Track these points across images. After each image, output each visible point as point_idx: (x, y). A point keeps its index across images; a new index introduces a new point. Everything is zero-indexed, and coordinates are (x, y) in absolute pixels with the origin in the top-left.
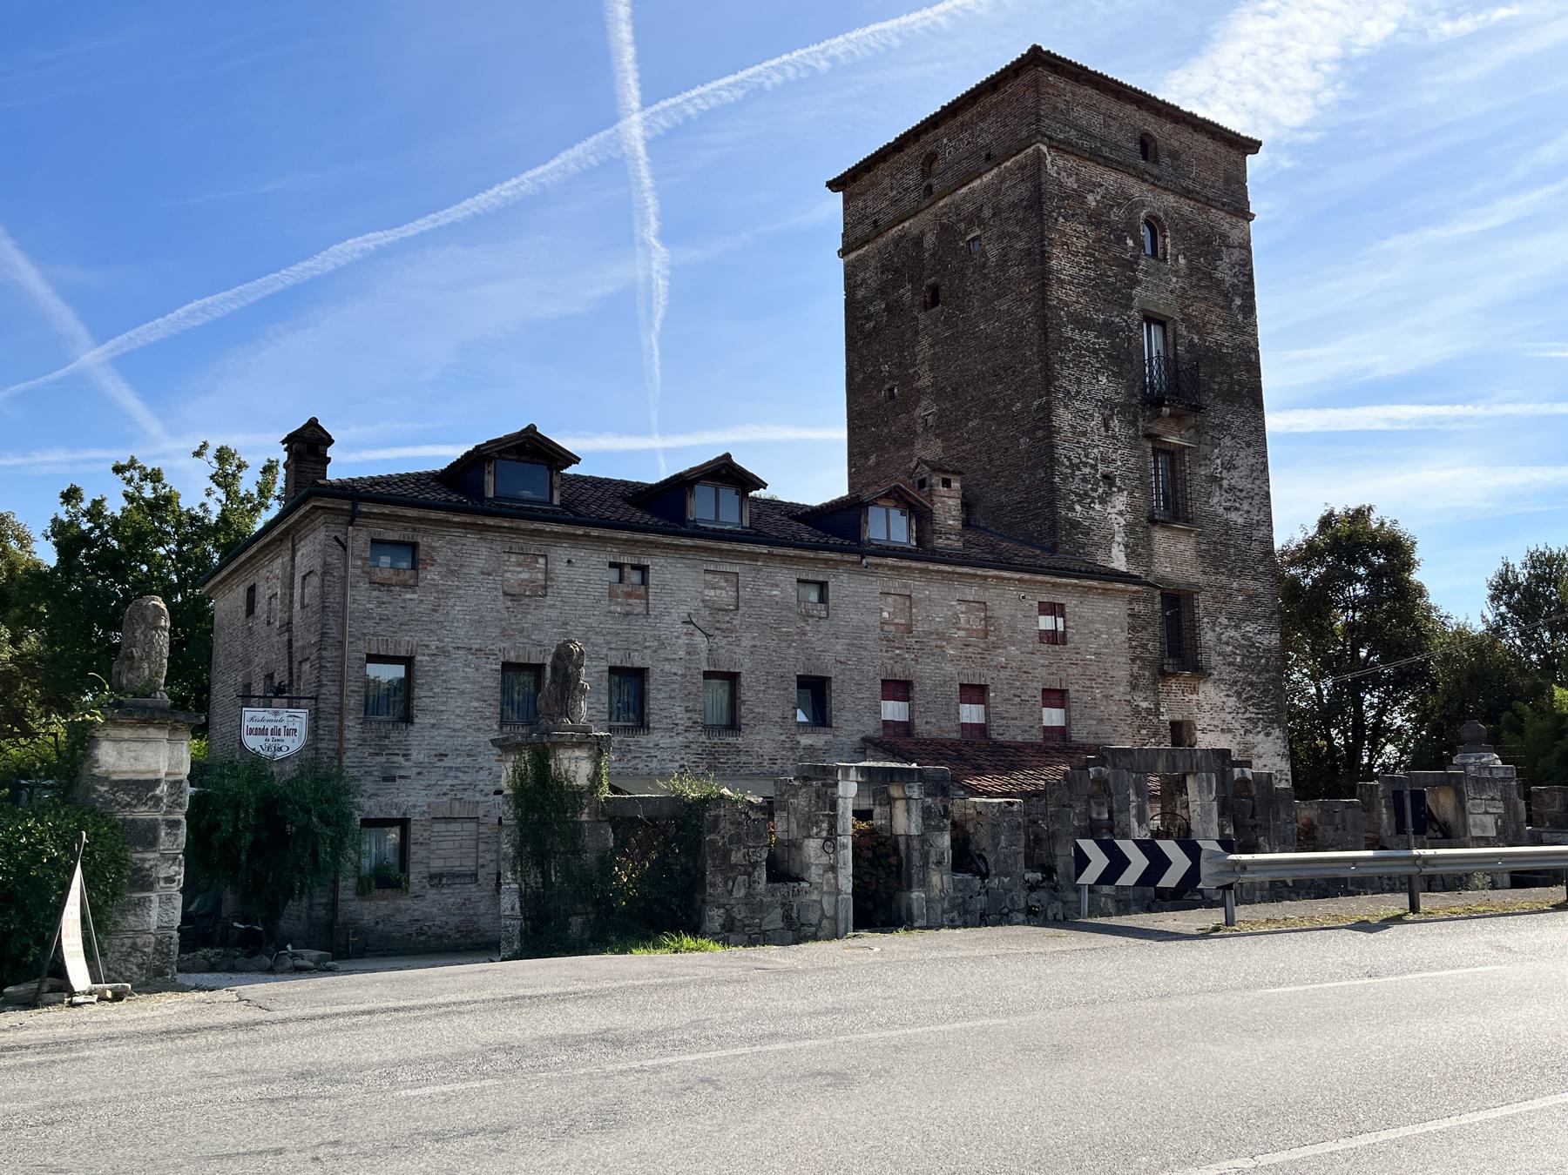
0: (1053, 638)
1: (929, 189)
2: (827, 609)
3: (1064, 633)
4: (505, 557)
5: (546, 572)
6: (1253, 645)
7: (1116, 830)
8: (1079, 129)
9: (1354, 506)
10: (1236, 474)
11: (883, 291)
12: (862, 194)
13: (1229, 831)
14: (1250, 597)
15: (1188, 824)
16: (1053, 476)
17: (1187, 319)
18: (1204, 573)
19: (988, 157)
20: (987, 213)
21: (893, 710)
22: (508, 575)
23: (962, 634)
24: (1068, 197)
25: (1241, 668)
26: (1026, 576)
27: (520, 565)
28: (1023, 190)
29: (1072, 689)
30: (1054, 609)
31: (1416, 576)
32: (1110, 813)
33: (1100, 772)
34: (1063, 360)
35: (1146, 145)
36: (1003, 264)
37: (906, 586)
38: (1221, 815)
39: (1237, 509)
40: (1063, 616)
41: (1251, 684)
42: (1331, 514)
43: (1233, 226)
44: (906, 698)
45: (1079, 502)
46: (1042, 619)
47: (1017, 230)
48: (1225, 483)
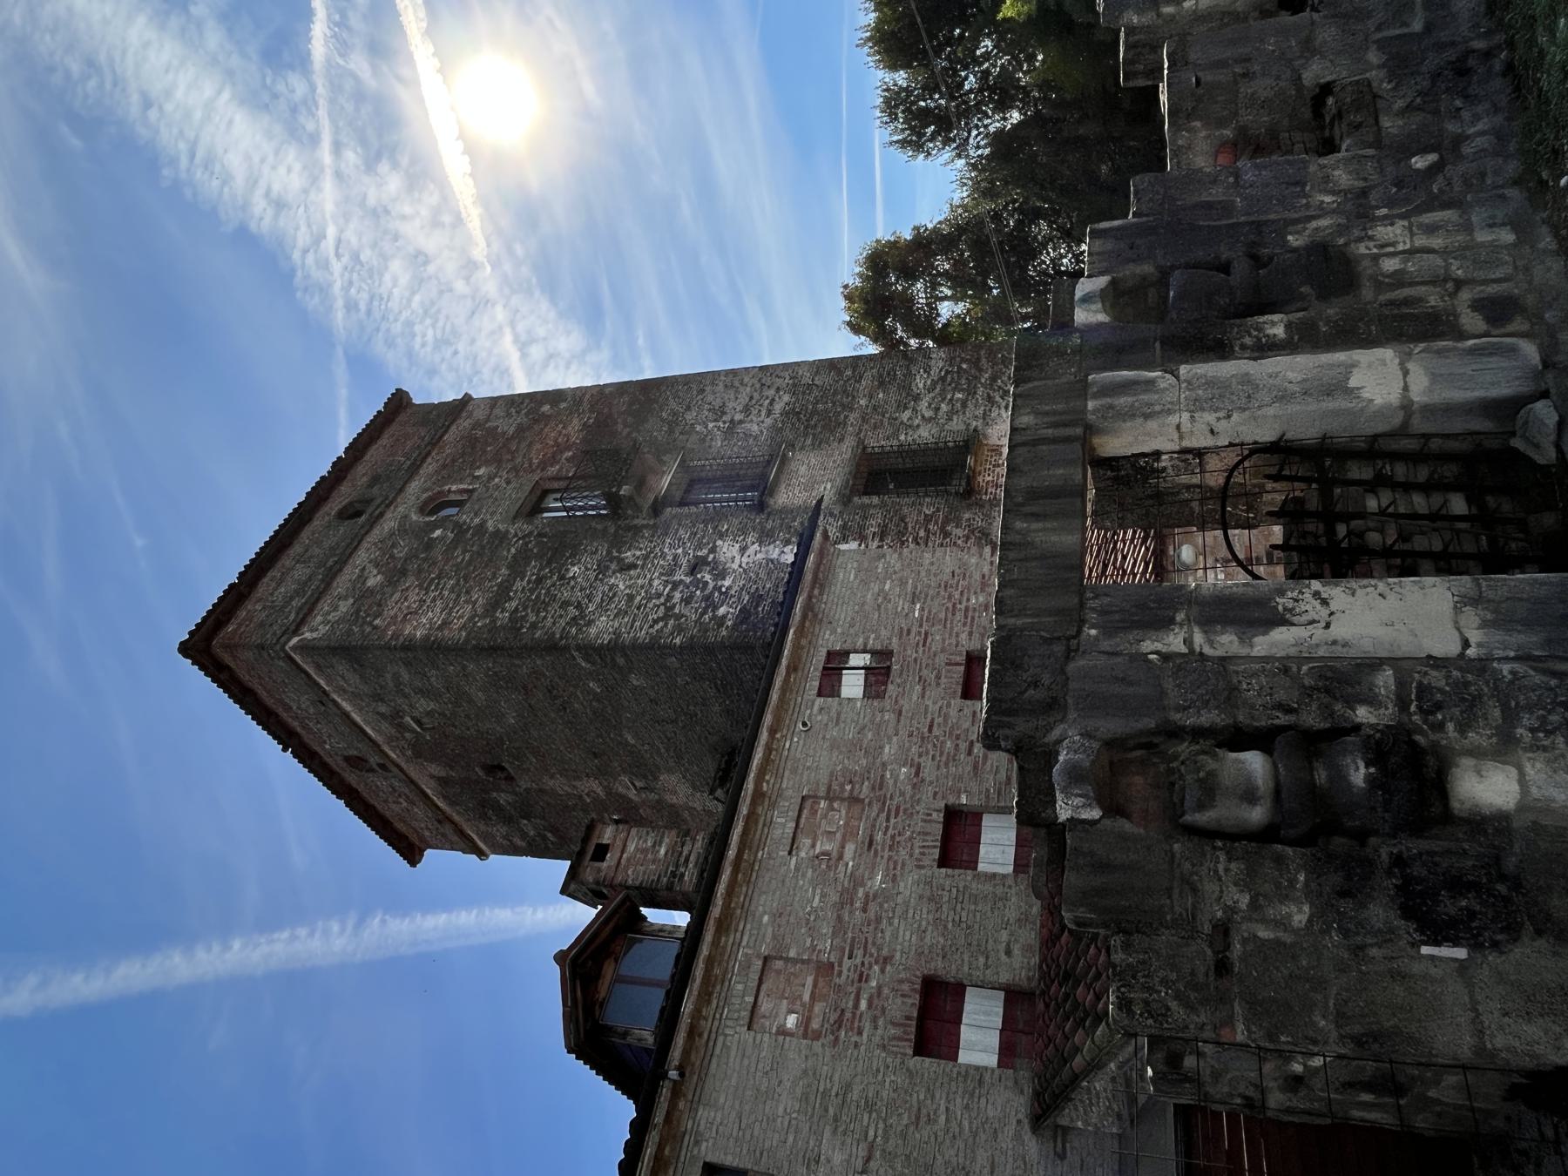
0: (877, 676)
3: (873, 653)
6: (943, 379)
7: (1311, 719)
8: (297, 593)
9: (843, 303)
10: (731, 405)
13: (1275, 325)
14: (882, 384)
15: (1259, 449)
16: (671, 647)
17: (543, 465)
18: (841, 440)
21: (980, 1034)
23: (850, 849)
25: (971, 392)
26: (768, 719)
28: (342, 667)
31: (908, 235)
32: (1239, 739)
33: (1076, 776)
34: (534, 626)
35: (350, 513)
37: (747, 966)
38: (1222, 351)
40: (847, 654)
41: (993, 379)
42: (849, 324)
44: (958, 991)
45: (715, 608)
46: (846, 692)
47: (388, 676)
48: (738, 417)
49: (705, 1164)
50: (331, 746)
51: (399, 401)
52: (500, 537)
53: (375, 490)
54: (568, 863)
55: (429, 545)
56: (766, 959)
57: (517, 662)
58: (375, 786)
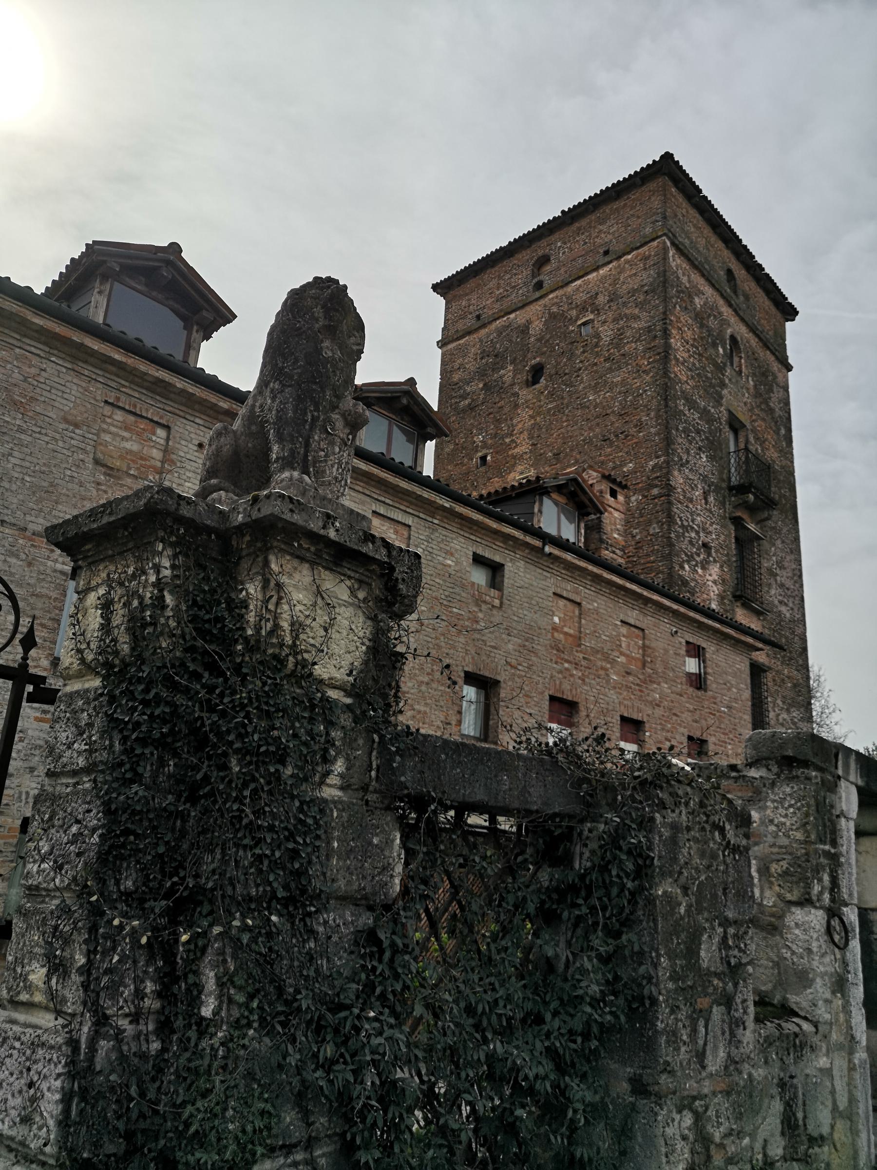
1: (539, 285)
2: (501, 598)
4: (107, 410)
5: (166, 451)
11: (482, 373)
12: (467, 295)
17: (754, 430)
19: (606, 253)
20: (602, 299)
22: (108, 438)
24: (683, 292)
27: (127, 428)
29: (711, 740)
30: (696, 651)
36: (618, 340)
39: (786, 605)
43: (780, 371)
45: (688, 562)
47: (637, 311)
49: (503, 565)
50: (562, 250)
51: (791, 312)
52: (718, 400)
53: (742, 298)
54: (359, 380)
55: (715, 345)
56: (579, 604)
57: (652, 414)
58: (519, 275)
